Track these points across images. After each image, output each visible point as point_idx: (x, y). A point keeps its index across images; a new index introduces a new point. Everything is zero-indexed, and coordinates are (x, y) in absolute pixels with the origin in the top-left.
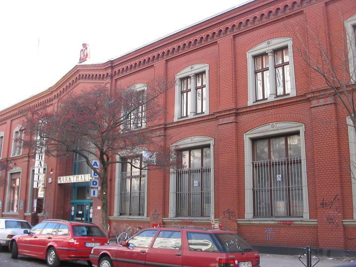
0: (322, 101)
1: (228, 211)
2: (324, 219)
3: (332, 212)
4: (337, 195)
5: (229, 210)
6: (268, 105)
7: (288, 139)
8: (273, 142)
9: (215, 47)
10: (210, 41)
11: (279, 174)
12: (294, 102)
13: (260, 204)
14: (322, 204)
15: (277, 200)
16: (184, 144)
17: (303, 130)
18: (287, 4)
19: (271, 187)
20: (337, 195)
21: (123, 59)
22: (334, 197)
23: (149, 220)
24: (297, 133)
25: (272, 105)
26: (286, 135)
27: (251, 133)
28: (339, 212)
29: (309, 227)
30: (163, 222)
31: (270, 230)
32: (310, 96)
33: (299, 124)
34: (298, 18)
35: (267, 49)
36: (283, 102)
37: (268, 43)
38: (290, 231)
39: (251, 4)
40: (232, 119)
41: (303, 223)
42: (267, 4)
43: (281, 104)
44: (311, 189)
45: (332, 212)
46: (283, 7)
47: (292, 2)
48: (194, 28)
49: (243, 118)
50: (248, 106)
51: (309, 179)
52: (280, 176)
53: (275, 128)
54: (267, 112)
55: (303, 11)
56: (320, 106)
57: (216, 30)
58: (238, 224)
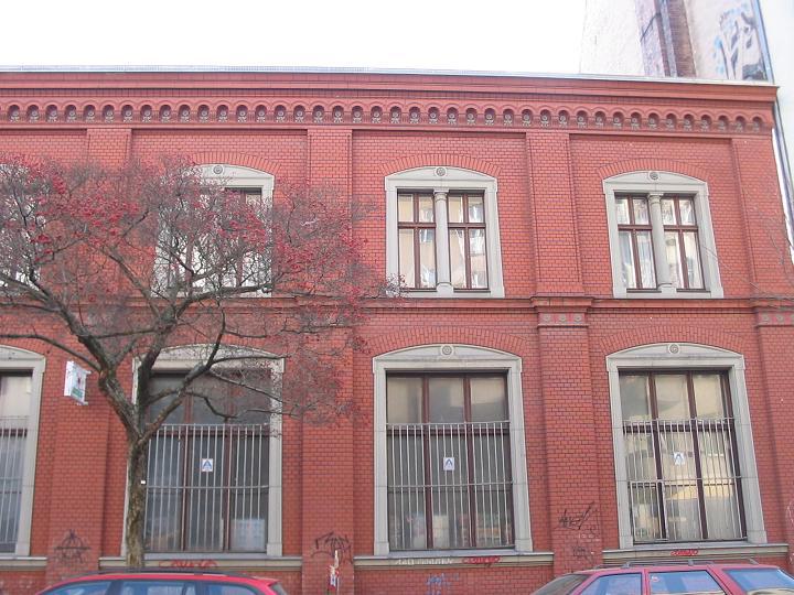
0: (563, 319)
1: (330, 538)
2: (568, 550)
3: (582, 537)
4: (593, 503)
5: (331, 534)
6: (442, 305)
7: (471, 383)
8: (435, 385)
9: (295, 142)
10: (722, 131)
11: (449, 455)
12: (501, 309)
13: (503, 520)
14: (564, 520)
15: (240, 516)
16: (475, 360)
17: (517, 367)
18: (37, 104)
19: (427, 482)
20: (593, 503)
21: (546, 87)
22: (587, 506)
23: (44, 564)
24: (28, 373)
25: (452, 305)
26: (466, 375)
27: (393, 357)
28: (596, 536)
29: (29, 572)
30: (100, 568)
31: (439, 579)
32: (541, 304)
33: (510, 356)
34: (510, 144)
35: (438, 184)
36: (478, 306)
37: (441, 174)
38: (488, 578)
39: (541, 83)
40: (578, 319)
41: (522, 560)
42: (399, 91)
43: (469, 309)
44: (535, 491)
45: (582, 537)
46: (235, 107)
47: (219, 104)
48: (386, 79)
49: (376, 325)
50: (615, 297)
51: (531, 470)
52: (452, 459)
53: (451, 356)
54: (433, 319)
55: (730, 139)
56: (574, 327)
57: (99, 102)
58: (355, 567)
